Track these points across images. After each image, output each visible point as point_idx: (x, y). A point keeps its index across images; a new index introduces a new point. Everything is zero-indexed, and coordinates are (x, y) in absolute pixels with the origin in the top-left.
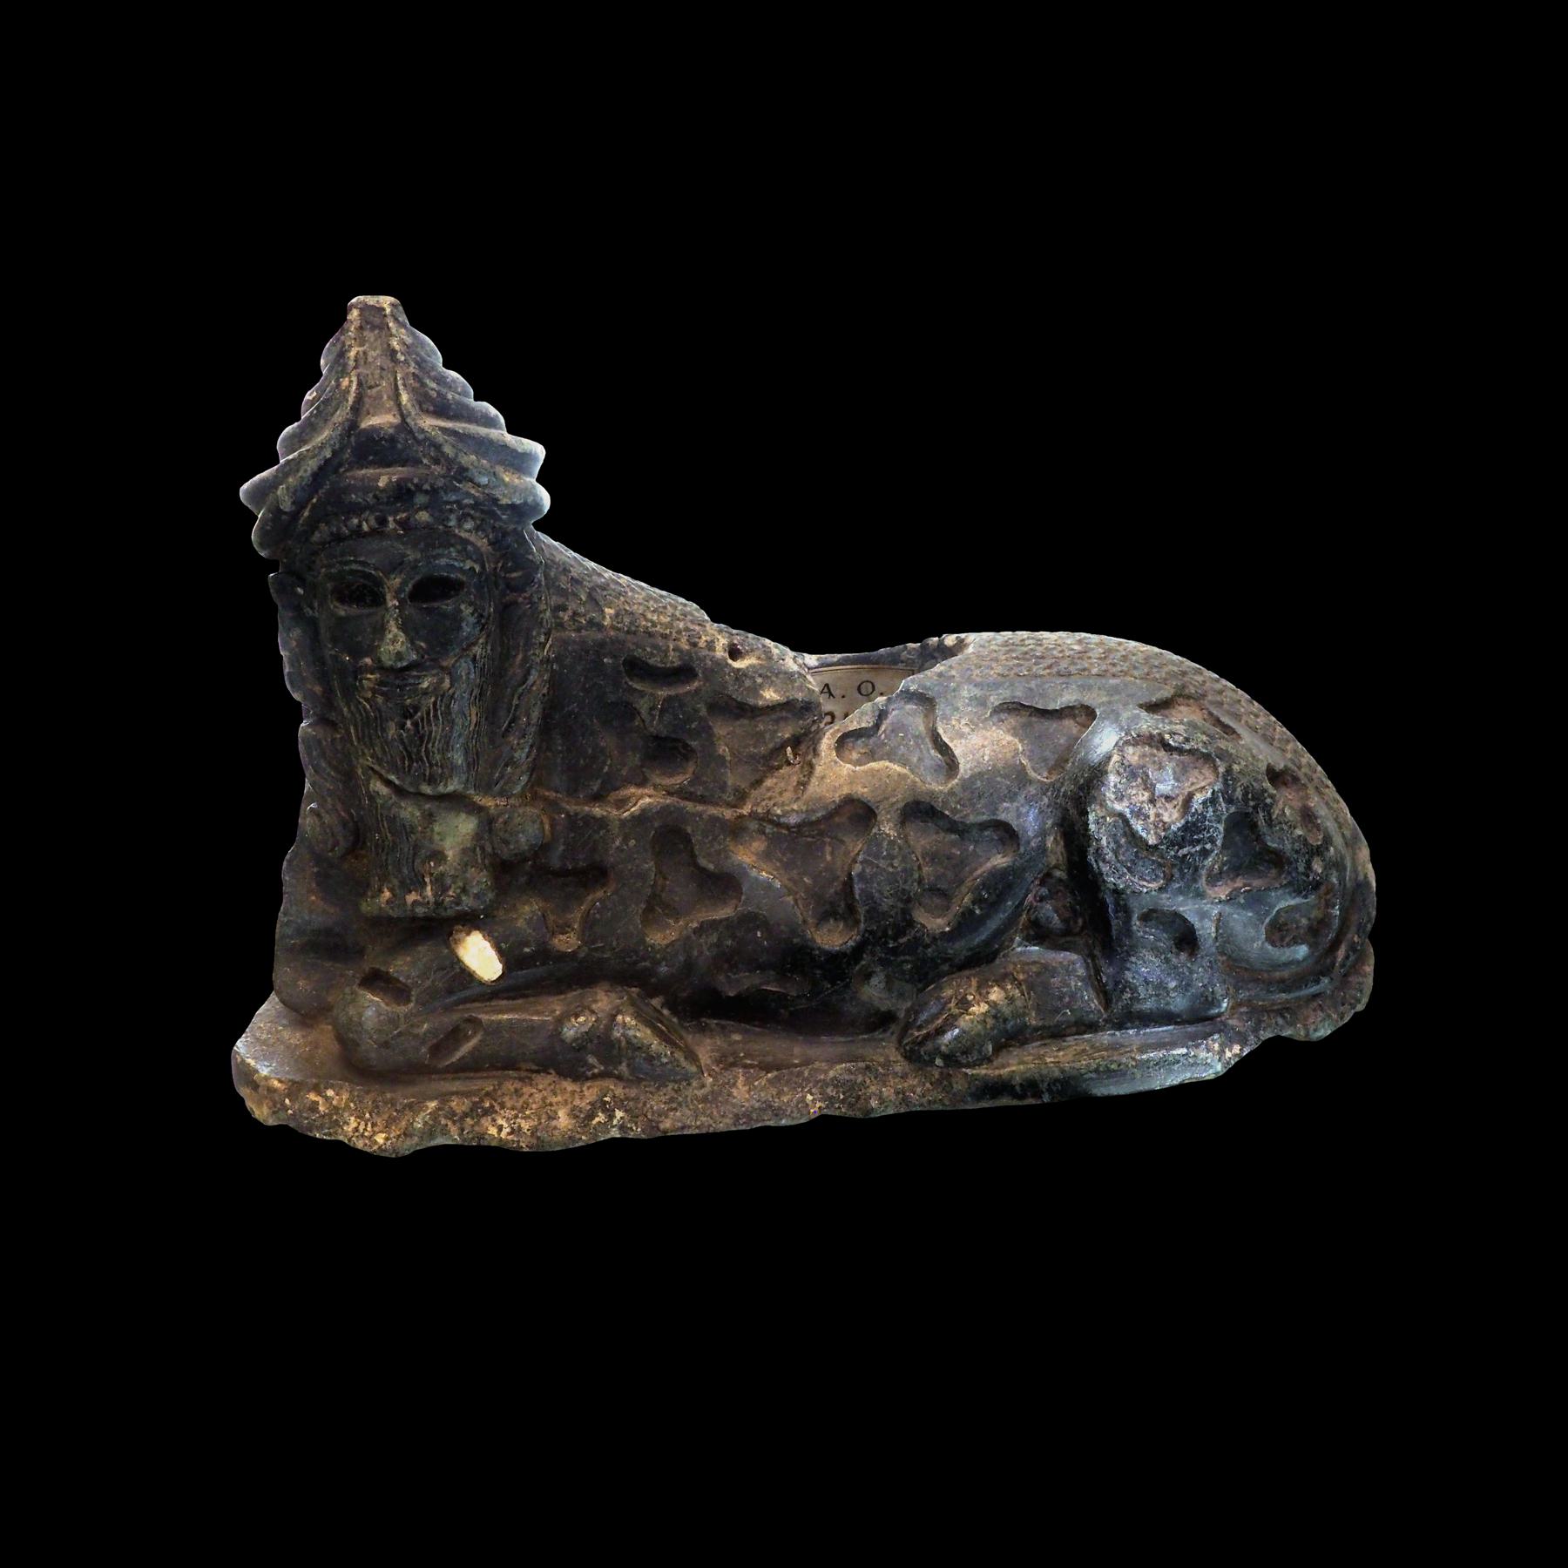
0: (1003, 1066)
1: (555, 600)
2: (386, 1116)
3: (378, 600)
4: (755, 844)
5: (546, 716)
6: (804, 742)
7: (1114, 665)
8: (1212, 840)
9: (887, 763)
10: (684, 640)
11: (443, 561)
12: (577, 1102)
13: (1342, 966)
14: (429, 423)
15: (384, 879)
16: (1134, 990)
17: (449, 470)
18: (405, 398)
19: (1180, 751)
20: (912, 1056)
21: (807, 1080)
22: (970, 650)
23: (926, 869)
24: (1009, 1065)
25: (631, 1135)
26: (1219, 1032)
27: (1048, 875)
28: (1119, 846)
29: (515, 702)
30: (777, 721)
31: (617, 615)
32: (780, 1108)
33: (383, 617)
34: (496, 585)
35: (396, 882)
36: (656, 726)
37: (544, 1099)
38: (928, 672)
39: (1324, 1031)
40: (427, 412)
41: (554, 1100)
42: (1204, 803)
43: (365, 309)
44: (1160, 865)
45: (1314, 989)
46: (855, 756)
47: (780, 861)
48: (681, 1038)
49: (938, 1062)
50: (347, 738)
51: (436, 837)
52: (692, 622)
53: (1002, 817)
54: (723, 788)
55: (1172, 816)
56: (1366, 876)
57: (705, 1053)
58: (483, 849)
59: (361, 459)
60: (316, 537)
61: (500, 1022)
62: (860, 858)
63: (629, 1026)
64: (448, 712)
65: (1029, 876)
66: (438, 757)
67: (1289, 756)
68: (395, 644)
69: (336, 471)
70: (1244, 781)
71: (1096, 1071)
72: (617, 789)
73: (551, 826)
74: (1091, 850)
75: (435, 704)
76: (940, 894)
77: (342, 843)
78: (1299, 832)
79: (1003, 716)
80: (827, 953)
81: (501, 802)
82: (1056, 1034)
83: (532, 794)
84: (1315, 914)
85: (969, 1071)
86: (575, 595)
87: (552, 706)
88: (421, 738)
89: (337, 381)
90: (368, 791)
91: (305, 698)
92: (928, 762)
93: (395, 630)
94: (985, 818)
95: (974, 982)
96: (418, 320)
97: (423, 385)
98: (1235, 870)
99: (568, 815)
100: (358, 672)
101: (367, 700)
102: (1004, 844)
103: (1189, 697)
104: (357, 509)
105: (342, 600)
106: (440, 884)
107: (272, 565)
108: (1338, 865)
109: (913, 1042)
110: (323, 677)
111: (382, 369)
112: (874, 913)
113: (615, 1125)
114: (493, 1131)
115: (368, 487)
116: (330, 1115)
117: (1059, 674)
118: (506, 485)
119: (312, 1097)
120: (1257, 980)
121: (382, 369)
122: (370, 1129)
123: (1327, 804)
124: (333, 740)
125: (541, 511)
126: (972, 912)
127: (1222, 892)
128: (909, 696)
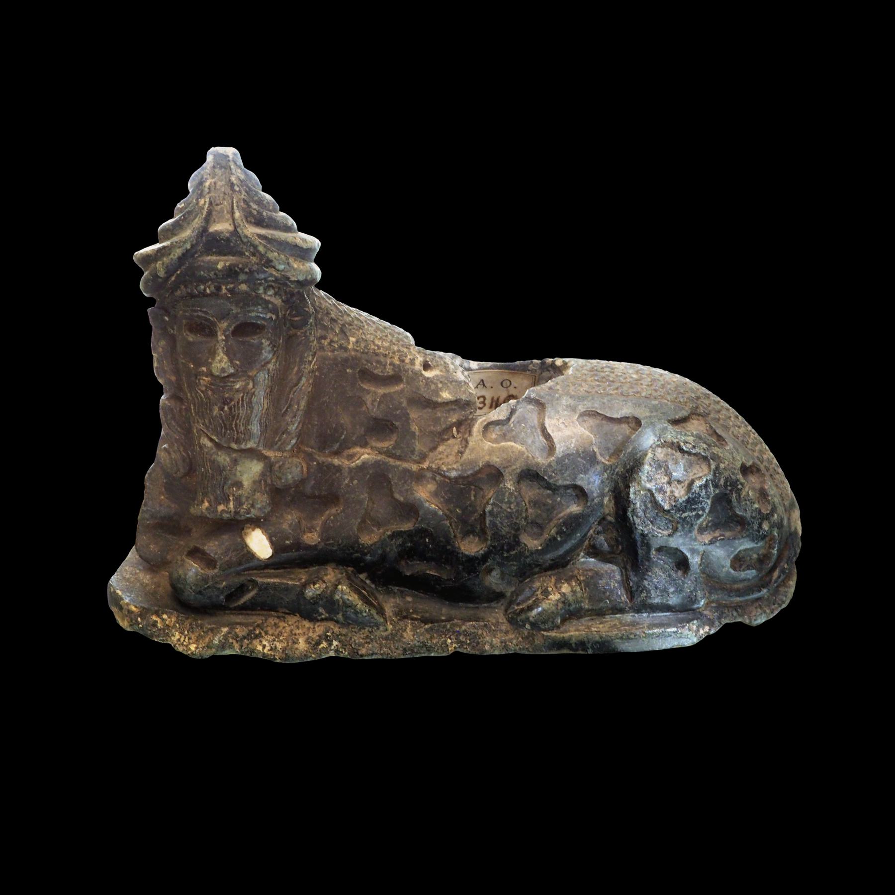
0: (566, 632)
1: (319, 333)
2: (197, 634)
3: (212, 334)
4: (429, 486)
5: (309, 404)
6: (464, 425)
7: (656, 391)
8: (703, 509)
9: (512, 444)
10: (396, 358)
11: (253, 314)
12: (311, 634)
13: (776, 582)
14: (251, 231)
15: (205, 494)
16: (648, 592)
17: (261, 260)
18: (237, 214)
19: (689, 453)
20: (512, 621)
21: (448, 630)
22: (570, 371)
23: (530, 511)
24: (569, 631)
25: (342, 655)
26: (697, 619)
27: (604, 519)
28: (647, 508)
29: (291, 396)
30: (449, 411)
31: (357, 342)
32: (431, 647)
33: (215, 345)
34: (285, 324)
35: (212, 497)
36: (376, 412)
37: (291, 631)
38: (543, 386)
39: (761, 620)
40: (250, 222)
41: (297, 632)
42: (700, 487)
43: (216, 155)
44: (670, 521)
45: (756, 595)
46: (494, 436)
47: (444, 498)
48: (376, 598)
49: (528, 626)
50: (188, 410)
51: (238, 474)
52: (402, 346)
53: (579, 483)
54: (413, 452)
55: (680, 493)
56: (796, 529)
57: (389, 610)
58: (265, 481)
59: (208, 251)
60: (178, 293)
61: (268, 584)
62: (491, 501)
63: (346, 593)
64: (250, 402)
65: (592, 520)
66: (242, 428)
67: (756, 454)
68: (221, 363)
69: (192, 256)
70: (726, 474)
71: (621, 638)
72: (349, 448)
73: (307, 468)
74: (630, 509)
75: (243, 397)
76: (538, 526)
77: (182, 470)
78: (756, 506)
79: (586, 418)
80: (467, 556)
81: (279, 454)
82: (599, 613)
83: (297, 451)
84: (762, 552)
85: (545, 633)
86: (332, 329)
87: (313, 398)
88: (233, 417)
89: (197, 200)
90: (199, 443)
92: (537, 444)
93: (222, 354)
94: (568, 483)
95: (553, 580)
96: (249, 163)
97: (249, 206)
98: (715, 525)
99: (318, 463)
100: (197, 375)
101: (202, 392)
102: (578, 499)
103: (699, 415)
104: (203, 280)
105: (191, 330)
106: (239, 501)
107: (151, 302)
108: (780, 526)
109: (514, 613)
110: (177, 372)
111: (225, 194)
112: (496, 536)
113: (332, 649)
114: (260, 648)
115: (211, 267)
116: (164, 630)
117: (622, 394)
118: (295, 270)
119: (154, 618)
120: (723, 589)
121: (225, 194)
122: (189, 641)
123: (776, 485)
124: (181, 409)
125: (315, 249)
126: (555, 539)
127: (707, 538)
128: (530, 400)
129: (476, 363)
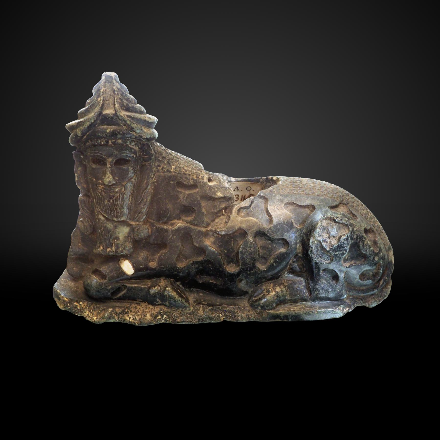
0: (278, 310)
1: (157, 164)
2: (97, 312)
3: (104, 164)
4: (211, 239)
5: (152, 199)
6: (228, 209)
7: (322, 192)
8: (346, 250)
9: (252, 218)
10: (195, 176)
11: (125, 154)
12: (153, 312)
13: (381, 286)
14: (123, 113)
15: (101, 243)
16: (319, 291)
17: (128, 128)
18: (117, 105)
19: (339, 223)
20: (252, 305)
21: (220, 310)
22: (280, 183)
23: (261, 251)
24: (280, 310)
25: (168, 322)
26: (343, 304)
27: (297, 255)
28: (318, 250)
29: (143, 195)
30: (221, 202)
31: (176, 168)
32: (212, 318)
33: (106, 170)
34: (140, 159)
35: (104, 245)
36: (185, 202)
37: (143, 310)
38: (267, 190)
39: (374, 305)
40: (123, 109)
41: (146, 311)
42: (344, 239)
43: (106, 76)
44: (330, 256)
45: (372, 293)
46: (243, 214)
47: (218, 245)
48: (185, 294)
49: (259, 308)
50: (92, 201)
51: (117, 233)
52: (198, 170)
53: (285, 237)
54: (203, 222)
55: (334, 242)
56: (391, 260)
57: (191, 300)
58: (130, 237)
59: (102, 123)
60: (88, 144)
61: (132, 287)
62: (242, 246)
63: (170, 291)
64: (123, 198)
65: (291, 255)
66: (119, 211)
67: (372, 223)
68: (109, 178)
69: (95, 126)
70: (357, 233)
71: (306, 314)
72: (172, 220)
73: (151, 230)
74: (310, 250)
75: (119, 195)
76: (265, 259)
77: (89, 231)
78: (372, 249)
79: (288, 206)
80: (229, 273)
81: (137, 223)
82: (295, 302)
83: (146, 222)
84: (374, 271)
85: (268, 311)
86: (163, 162)
87: (154, 196)
88: (115, 205)
89: (97, 98)
90: (98, 218)
91: (81, 188)
92: (264, 218)
93: (109, 174)
94: (279, 237)
95: (272, 285)
97: (122, 101)
98: (352, 258)
99: (156, 228)
100: (97, 184)
101: (99, 193)
102: (284, 245)
103: (344, 204)
104: (100, 138)
105: (94, 162)
106: (117, 247)
107: (74, 148)
108: (383, 258)
109: (253, 301)
110: (87, 183)
111: (110, 95)
112: (244, 263)
113: (163, 319)
114: (128, 319)
115: (104, 131)
116: (81, 310)
117: (306, 194)
118: (145, 133)
119: (76, 304)
120: (355, 290)
121: (110, 95)
122: (93, 315)
123: (382, 239)
124: (89, 201)
125: (155, 123)
126: (273, 265)
127: (347, 264)
128: (260, 197)
129: (234, 178)
